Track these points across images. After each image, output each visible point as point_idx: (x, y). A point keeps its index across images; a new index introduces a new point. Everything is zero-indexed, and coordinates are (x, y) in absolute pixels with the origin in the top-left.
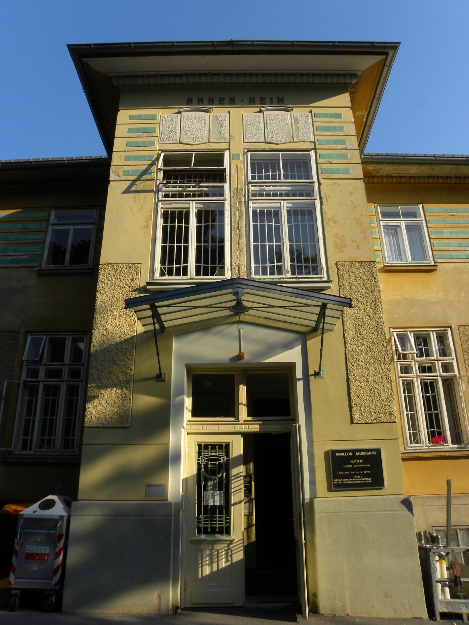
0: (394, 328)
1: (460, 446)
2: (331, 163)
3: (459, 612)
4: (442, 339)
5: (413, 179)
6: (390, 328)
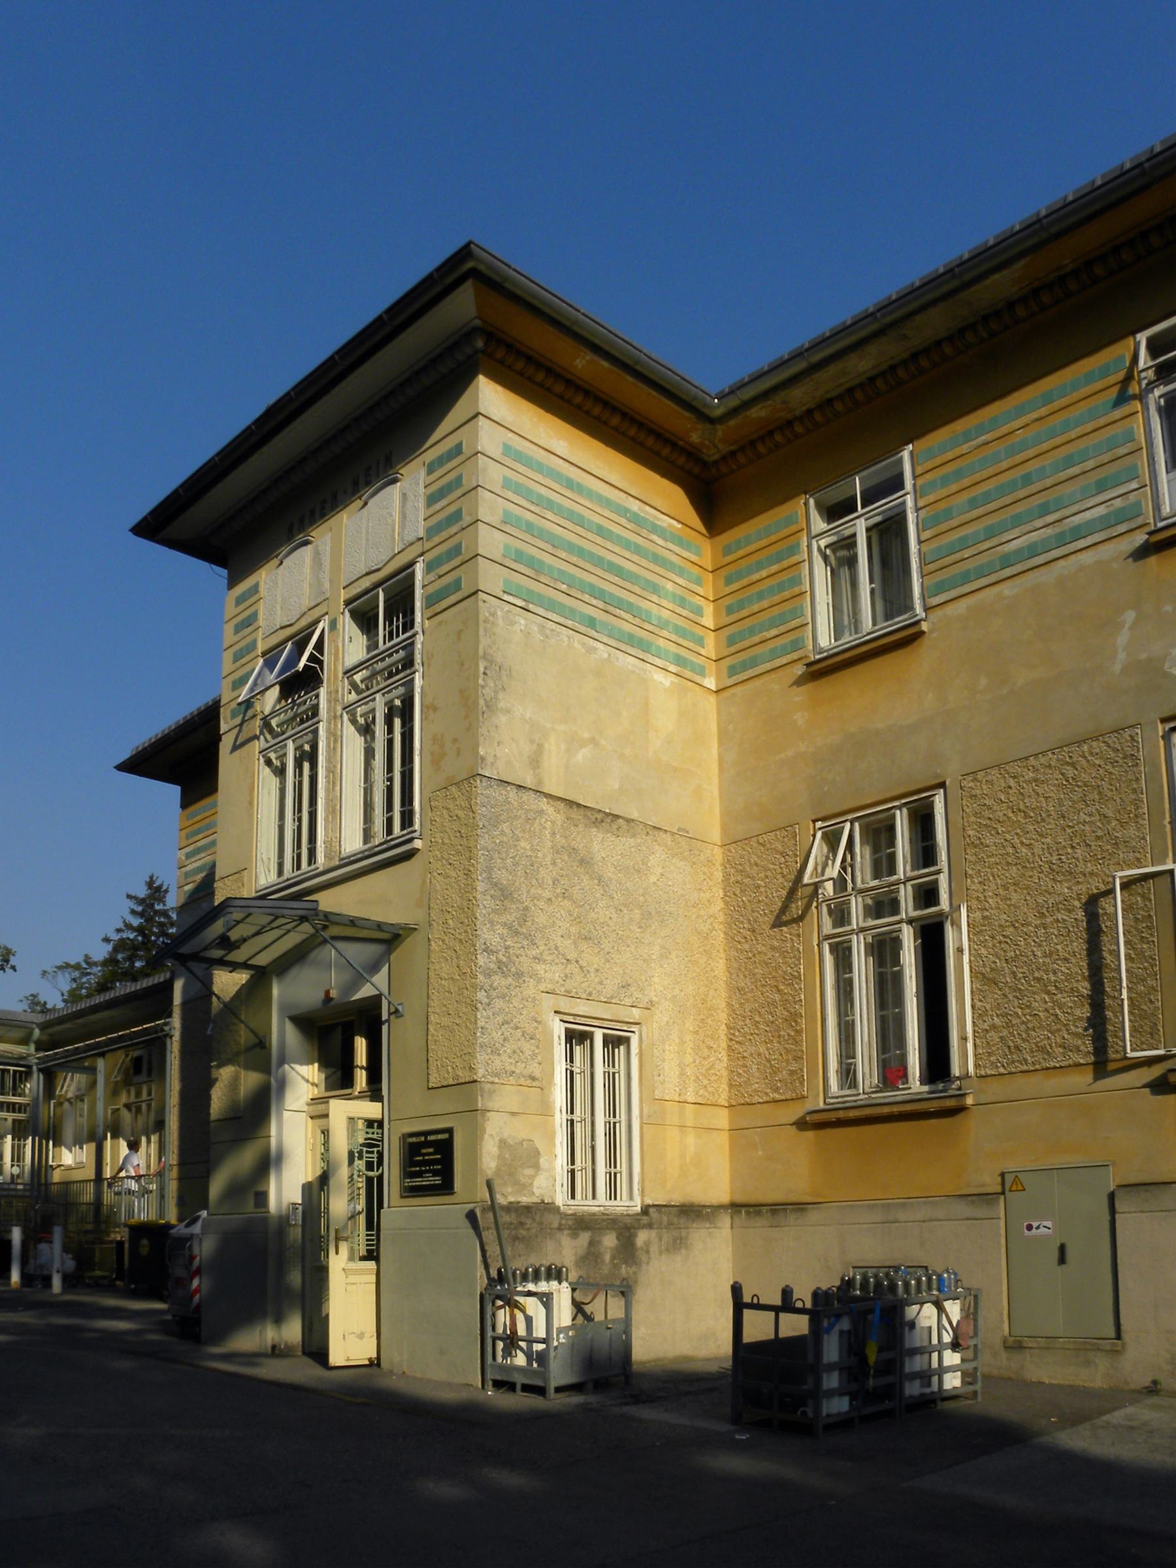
0: (823, 819)
1: (933, 1087)
2: (440, 577)
3: (511, 1380)
4: (923, 822)
5: (880, 383)
6: (814, 821)
